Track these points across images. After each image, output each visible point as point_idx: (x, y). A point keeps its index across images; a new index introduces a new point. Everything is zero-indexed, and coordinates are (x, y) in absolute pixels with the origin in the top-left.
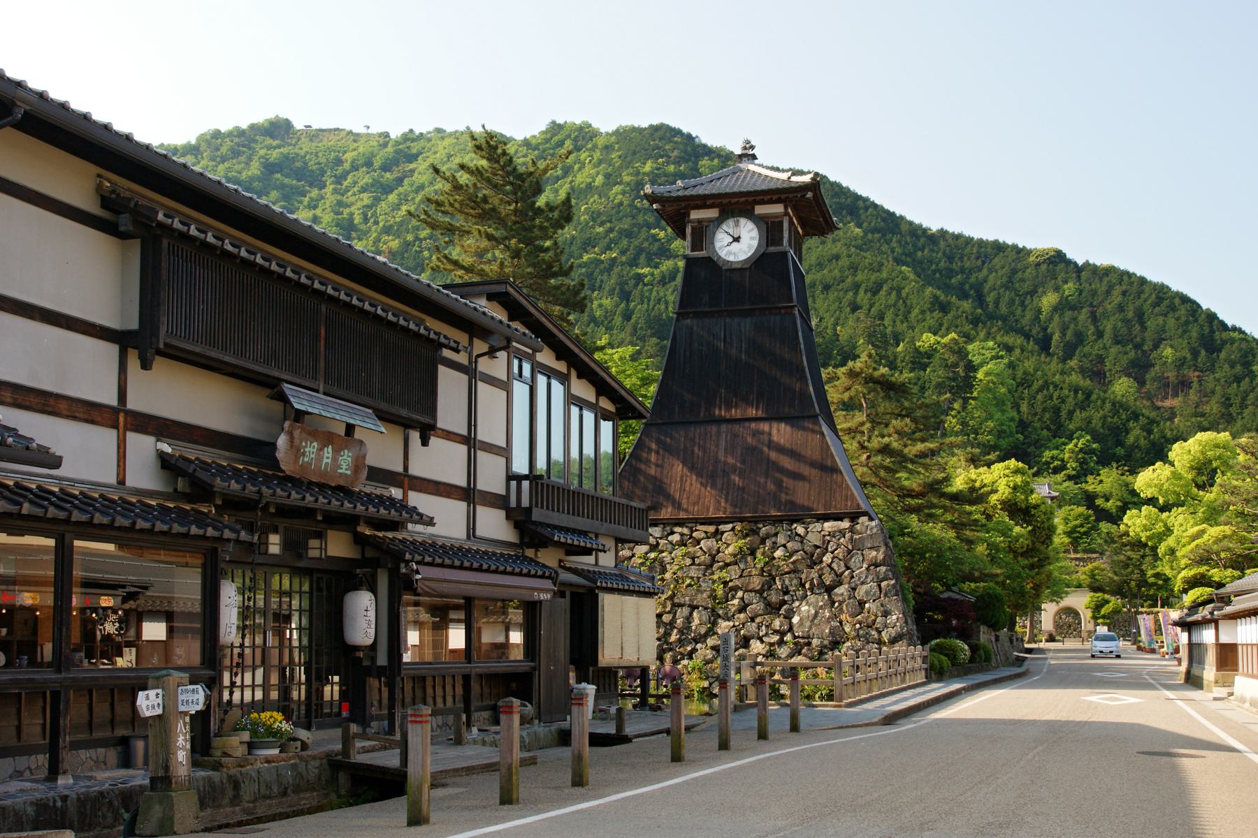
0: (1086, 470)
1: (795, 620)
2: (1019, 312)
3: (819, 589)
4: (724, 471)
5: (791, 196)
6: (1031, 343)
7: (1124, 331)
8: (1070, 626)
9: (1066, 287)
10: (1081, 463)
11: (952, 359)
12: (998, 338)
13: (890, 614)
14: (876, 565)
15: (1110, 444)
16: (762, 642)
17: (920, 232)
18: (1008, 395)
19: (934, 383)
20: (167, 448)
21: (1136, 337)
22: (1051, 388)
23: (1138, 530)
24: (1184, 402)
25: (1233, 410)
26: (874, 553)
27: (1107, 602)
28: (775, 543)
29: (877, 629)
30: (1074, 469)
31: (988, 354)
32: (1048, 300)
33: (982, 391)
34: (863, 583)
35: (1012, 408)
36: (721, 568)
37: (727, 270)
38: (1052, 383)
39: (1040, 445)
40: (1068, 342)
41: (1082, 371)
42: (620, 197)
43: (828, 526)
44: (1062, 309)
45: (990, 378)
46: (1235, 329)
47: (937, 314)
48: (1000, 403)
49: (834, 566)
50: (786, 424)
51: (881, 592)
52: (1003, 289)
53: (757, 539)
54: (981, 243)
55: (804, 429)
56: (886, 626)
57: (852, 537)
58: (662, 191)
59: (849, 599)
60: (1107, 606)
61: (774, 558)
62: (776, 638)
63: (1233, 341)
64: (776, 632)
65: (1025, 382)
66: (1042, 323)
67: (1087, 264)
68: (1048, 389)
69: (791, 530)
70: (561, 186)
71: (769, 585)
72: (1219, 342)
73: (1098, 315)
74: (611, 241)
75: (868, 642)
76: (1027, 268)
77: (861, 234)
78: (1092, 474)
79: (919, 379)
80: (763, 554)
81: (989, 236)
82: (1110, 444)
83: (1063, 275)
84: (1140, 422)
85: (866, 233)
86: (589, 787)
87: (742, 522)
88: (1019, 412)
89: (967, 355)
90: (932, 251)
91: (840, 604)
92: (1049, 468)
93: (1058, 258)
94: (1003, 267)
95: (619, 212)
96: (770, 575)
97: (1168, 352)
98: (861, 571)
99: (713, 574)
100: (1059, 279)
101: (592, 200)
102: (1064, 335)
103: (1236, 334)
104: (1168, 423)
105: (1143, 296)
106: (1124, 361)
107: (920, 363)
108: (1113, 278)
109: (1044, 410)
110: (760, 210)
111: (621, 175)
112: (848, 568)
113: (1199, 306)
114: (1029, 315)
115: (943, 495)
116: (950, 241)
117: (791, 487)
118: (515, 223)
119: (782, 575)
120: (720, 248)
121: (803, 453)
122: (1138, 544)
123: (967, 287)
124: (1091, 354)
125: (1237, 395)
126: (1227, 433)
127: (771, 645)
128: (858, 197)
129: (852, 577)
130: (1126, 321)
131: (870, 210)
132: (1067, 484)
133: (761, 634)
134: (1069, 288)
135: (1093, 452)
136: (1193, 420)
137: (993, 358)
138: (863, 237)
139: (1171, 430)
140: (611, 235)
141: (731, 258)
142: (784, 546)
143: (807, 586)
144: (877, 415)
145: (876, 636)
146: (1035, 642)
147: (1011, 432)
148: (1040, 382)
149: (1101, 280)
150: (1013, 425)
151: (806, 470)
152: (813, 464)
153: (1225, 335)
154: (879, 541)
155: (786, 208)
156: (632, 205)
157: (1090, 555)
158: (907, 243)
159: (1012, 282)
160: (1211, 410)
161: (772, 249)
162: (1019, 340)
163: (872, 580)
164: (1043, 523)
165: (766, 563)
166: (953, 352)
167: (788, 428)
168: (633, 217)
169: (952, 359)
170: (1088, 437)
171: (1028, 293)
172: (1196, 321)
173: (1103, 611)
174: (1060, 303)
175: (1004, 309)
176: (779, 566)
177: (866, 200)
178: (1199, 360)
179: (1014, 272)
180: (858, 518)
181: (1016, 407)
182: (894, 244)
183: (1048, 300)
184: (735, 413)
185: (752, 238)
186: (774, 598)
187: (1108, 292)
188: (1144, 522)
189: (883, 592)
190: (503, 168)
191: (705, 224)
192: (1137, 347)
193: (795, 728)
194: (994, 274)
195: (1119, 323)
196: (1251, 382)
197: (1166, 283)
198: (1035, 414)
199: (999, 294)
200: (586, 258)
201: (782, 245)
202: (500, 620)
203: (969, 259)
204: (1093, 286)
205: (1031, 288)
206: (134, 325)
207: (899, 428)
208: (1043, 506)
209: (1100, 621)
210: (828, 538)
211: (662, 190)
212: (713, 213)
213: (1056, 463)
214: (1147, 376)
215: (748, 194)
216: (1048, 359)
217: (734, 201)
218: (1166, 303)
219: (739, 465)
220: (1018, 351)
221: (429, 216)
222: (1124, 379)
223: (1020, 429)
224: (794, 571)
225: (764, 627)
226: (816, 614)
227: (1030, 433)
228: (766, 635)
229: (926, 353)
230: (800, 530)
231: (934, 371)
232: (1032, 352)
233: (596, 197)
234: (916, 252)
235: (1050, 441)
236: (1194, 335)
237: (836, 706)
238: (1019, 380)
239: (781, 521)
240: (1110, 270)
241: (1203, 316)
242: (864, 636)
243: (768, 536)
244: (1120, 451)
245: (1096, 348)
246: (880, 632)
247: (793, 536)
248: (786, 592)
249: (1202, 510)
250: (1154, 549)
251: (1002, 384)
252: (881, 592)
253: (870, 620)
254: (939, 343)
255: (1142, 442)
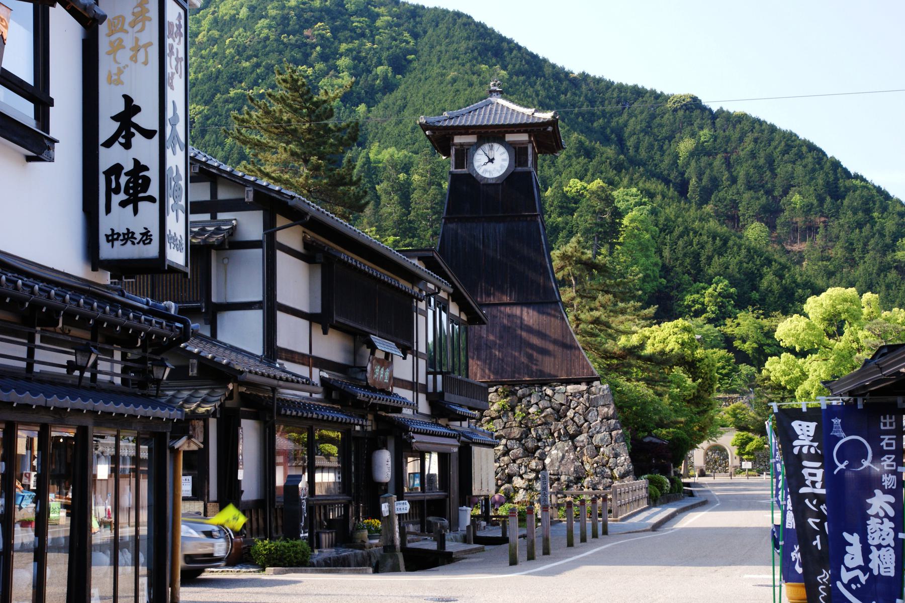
0: (725, 313)
1: (548, 461)
2: (657, 157)
3: (565, 437)
4: (486, 344)
5: (535, 129)
6: (672, 189)
7: (756, 177)
8: (716, 462)
9: (701, 133)
10: (720, 307)
11: (599, 205)
12: (641, 185)
13: (619, 456)
14: (608, 419)
15: (745, 288)
16: (522, 478)
17: (562, 76)
18: (652, 241)
19: (581, 227)
20: (326, 376)
21: (767, 183)
22: (691, 234)
23: (778, 375)
24: (812, 247)
25: (856, 254)
26: (606, 409)
27: (751, 440)
28: (529, 401)
29: (610, 467)
30: (713, 312)
31: (632, 201)
32: (685, 146)
33: (628, 237)
34: (598, 432)
35: (656, 252)
36: (488, 422)
37: (484, 185)
38: (692, 229)
39: (682, 289)
40: (704, 187)
41: (718, 215)
42: (266, 31)
43: (571, 388)
44: (698, 155)
45: (635, 224)
46: (857, 177)
47: (582, 160)
48: (644, 248)
49: (576, 419)
50: (533, 309)
51: (612, 439)
52: (642, 134)
53: (515, 399)
54: (621, 88)
55: (549, 314)
56: (616, 465)
57: (589, 397)
58: (433, 120)
59: (588, 444)
60: (751, 443)
61: (529, 414)
62: (533, 475)
63: (855, 188)
64: (532, 470)
65: (666, 229)
66: (679, 168)
67: (721, 111)
68: (688, 235)
69: (542, 392)
70: (204, 17)
71: (526, 434)
72: (842, 189)
73: (732, 161)
74: (259, 76)
75: (603, 478)
76: (664, 114)
77: (507, 77)
78: (730, 317)
79: (567, 224)
80: (521, 410)
81: (629, 80)
82: (745, 288)
83: (698, 121)
84: (773, 268)
85: (511, 75)
86: (550, 556)
87: (503, 385)
88: (662, 257)
89: (613, 202)
90: (574, 94)
91: (581, 449)
92: (690, 311)
93: (694, 105)
94: (642, 112)
95: (265, 47)
96: (527, 426)
97: (796, 198)
98: (596, 423)
99: (482, 425)
100: (695, 125)
101: (236, 33)
102: (701, 180)
103: (858, 182)
104: (797, 266)
105: (774, 144)
106: (756, 206)
107: (567, 208)
108: (746, 125)
109: (685, 255)
110: (510, 138)
111: (266, 8)
112: (586, 421)
113: (824, 154)
114: (667, 160)
115: (640, 357)
116: (592, 85)
117: (540, 360)
118: (310, 140)
119: (536, 426)
120: (478, 167)
121: (548, 333)
122: (779, 387)
123: (608, 131)
124: (725, 199)
125: (859, 240)
126: (854, 289)
127: (530, 480)
128: (502, 39)
129: (590, 428)
130: (758, 167)
131: (515, 52)
132: (707, 327)
133: (521, 472)
134: (705, 134)
135: (730, 296)
136: (820, 263)
137: (637, 204)
138: (509, 80)
139: (801, 275)
140: (258, 71)
141: (487, 175)
142: (537, 404)
143: (556, 435)
144: (585, 290)
145: (609, 473)
146: (689, 477)
147: (654, 276)
148: (681, 228)
149: (734, 127)
150: (657, 269)
151: (551, 347)
152: (555, 342)
153: (848, 183)
154: (609, 400)
155: (530, 137)
156: (278, 40)
157: (731, 395)
158: (550, 87)
159: (650, 127)
160: (836, 254)
161: (520, 169)
162: (661, 187)
163: (605, 430)
164: (706, 374)
165: (523, 418)
166: (601, 199)
167: (535, 313)
168: (281, 53)
169: (599, 205)
170: (726, 282)
171: (666, 138)
172: (822, 168)
173: (748, 448)
174: (696, 148)
175: (643, 154)
176: (533, 420)
177: (510, 42)
178: (825, 206)
179: (653, 117)
180: (592, 382)
181: (659, 252)
182: (538, 87)
183: (685, 146)
184: (492, 300)
185: (504, 160)
186: (530, 444)
187: (741, 139)
188: (783, 367)
189: (614, 439)
190: (301, 96)
191: (466, 147)
192: (768, 192)
193: (605, 532)
194: (634, 119)
195: (752, 170)
196: (872, 228)
197: (794, 131)
198: (677, 259)
199: (638, 138)
200: (232, 93)
201: (527, 166)
202: (294, 464)
203: (610, 103)
204: (727, 133)
205: (669, 133)
206: (318, 310)
207: (604, 302)
208: (706, 360)
209: (745, 457)
210: (571, 398)
211: (432, 119)
212: (472, 139)
213: (697, 306)
214: (778, 221)
215: (503, 126)
216: (687, 206)
217: (490, 131)
218: (794, 150)
219: (498, 341)
220: (659, 197)
221: (241, 134)
222: (756, 224)
223: (662, 273)
224: (545, 423)
225: (523, 467)
226: (563, 456)
227: (673, 277)
228: (525, 473)
229: (573, 198)
230: (549, 392)
231: (581, 216)
232: (672, 198)
233: (241, 30)
234: (559, 95)
235: (691, 285)
236: (820, 182)
237: (614, 521)
238: (661, 226)
239: (533, 385)
240: (742, 118)
241: (828, 164)
242: (600, 473)
243: (524, 396)
244: (755, 295)
245: (731, 193)
246: (612, 470)
247: (543, 396)
248: (539, 439)
249: (833, 357)
250: (792, 391)
251: (647, 231)
252: (612, 439)
253: (604, 461)
254: (585, 188)
255: (775, 287)
